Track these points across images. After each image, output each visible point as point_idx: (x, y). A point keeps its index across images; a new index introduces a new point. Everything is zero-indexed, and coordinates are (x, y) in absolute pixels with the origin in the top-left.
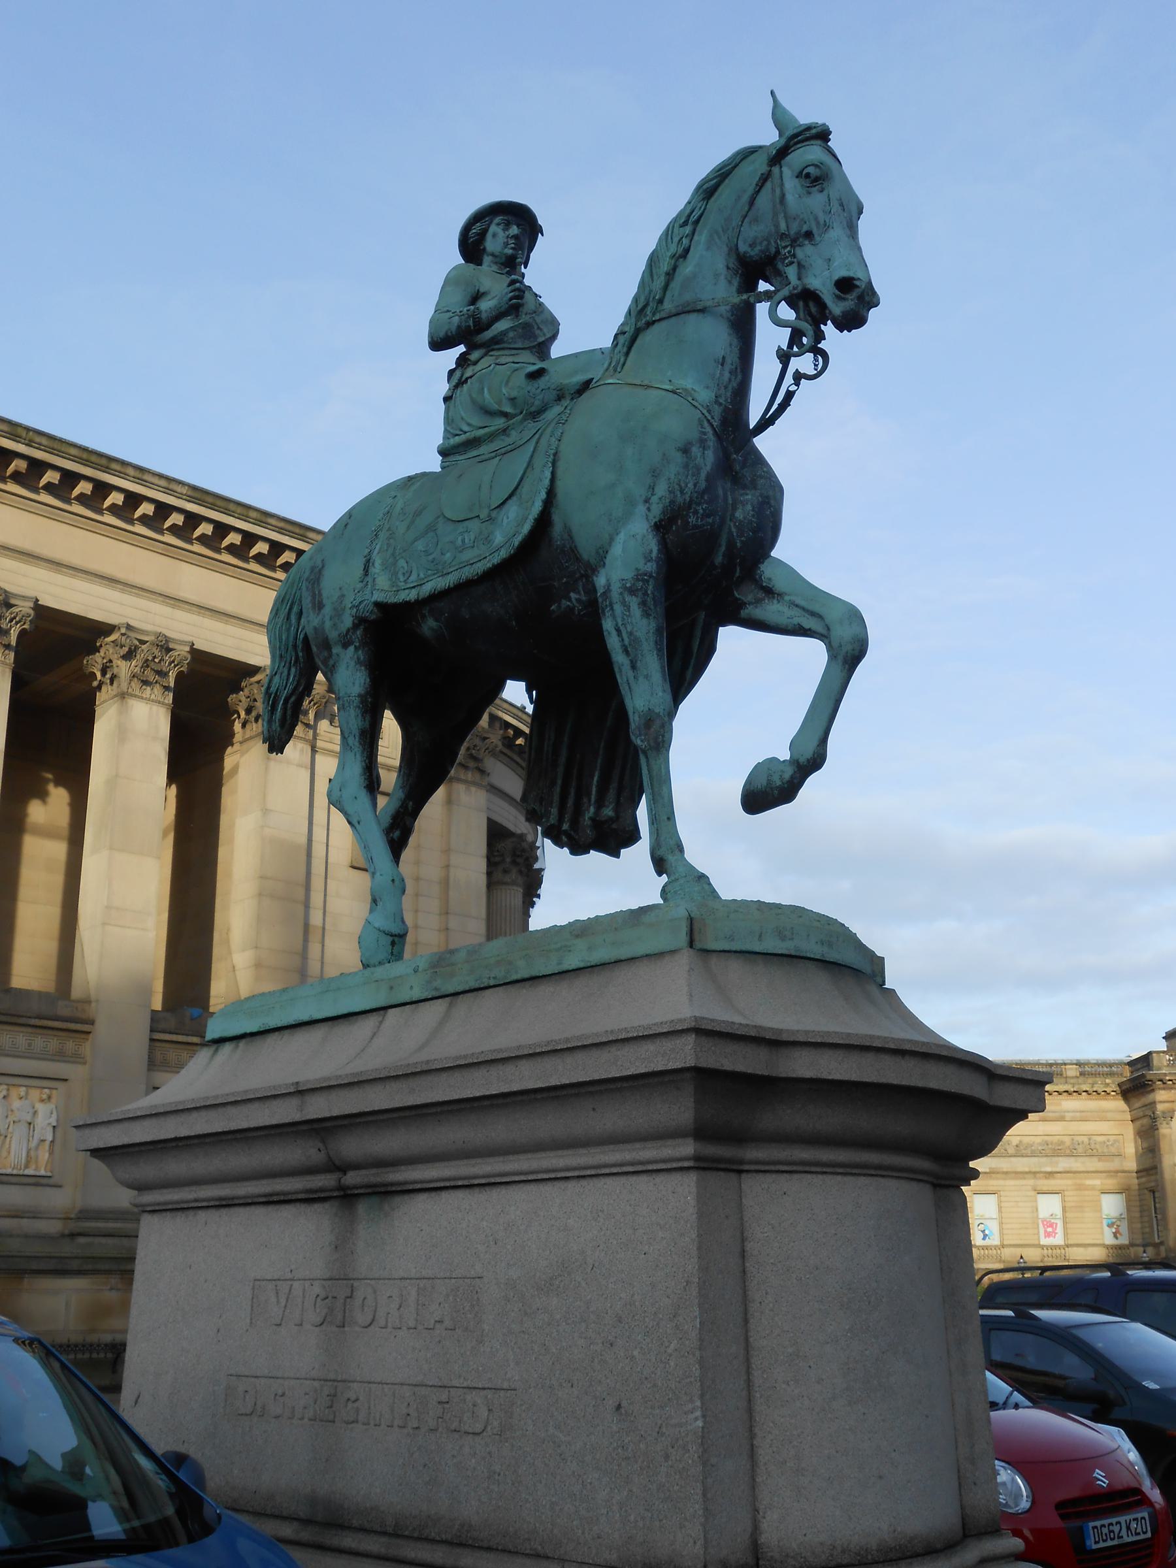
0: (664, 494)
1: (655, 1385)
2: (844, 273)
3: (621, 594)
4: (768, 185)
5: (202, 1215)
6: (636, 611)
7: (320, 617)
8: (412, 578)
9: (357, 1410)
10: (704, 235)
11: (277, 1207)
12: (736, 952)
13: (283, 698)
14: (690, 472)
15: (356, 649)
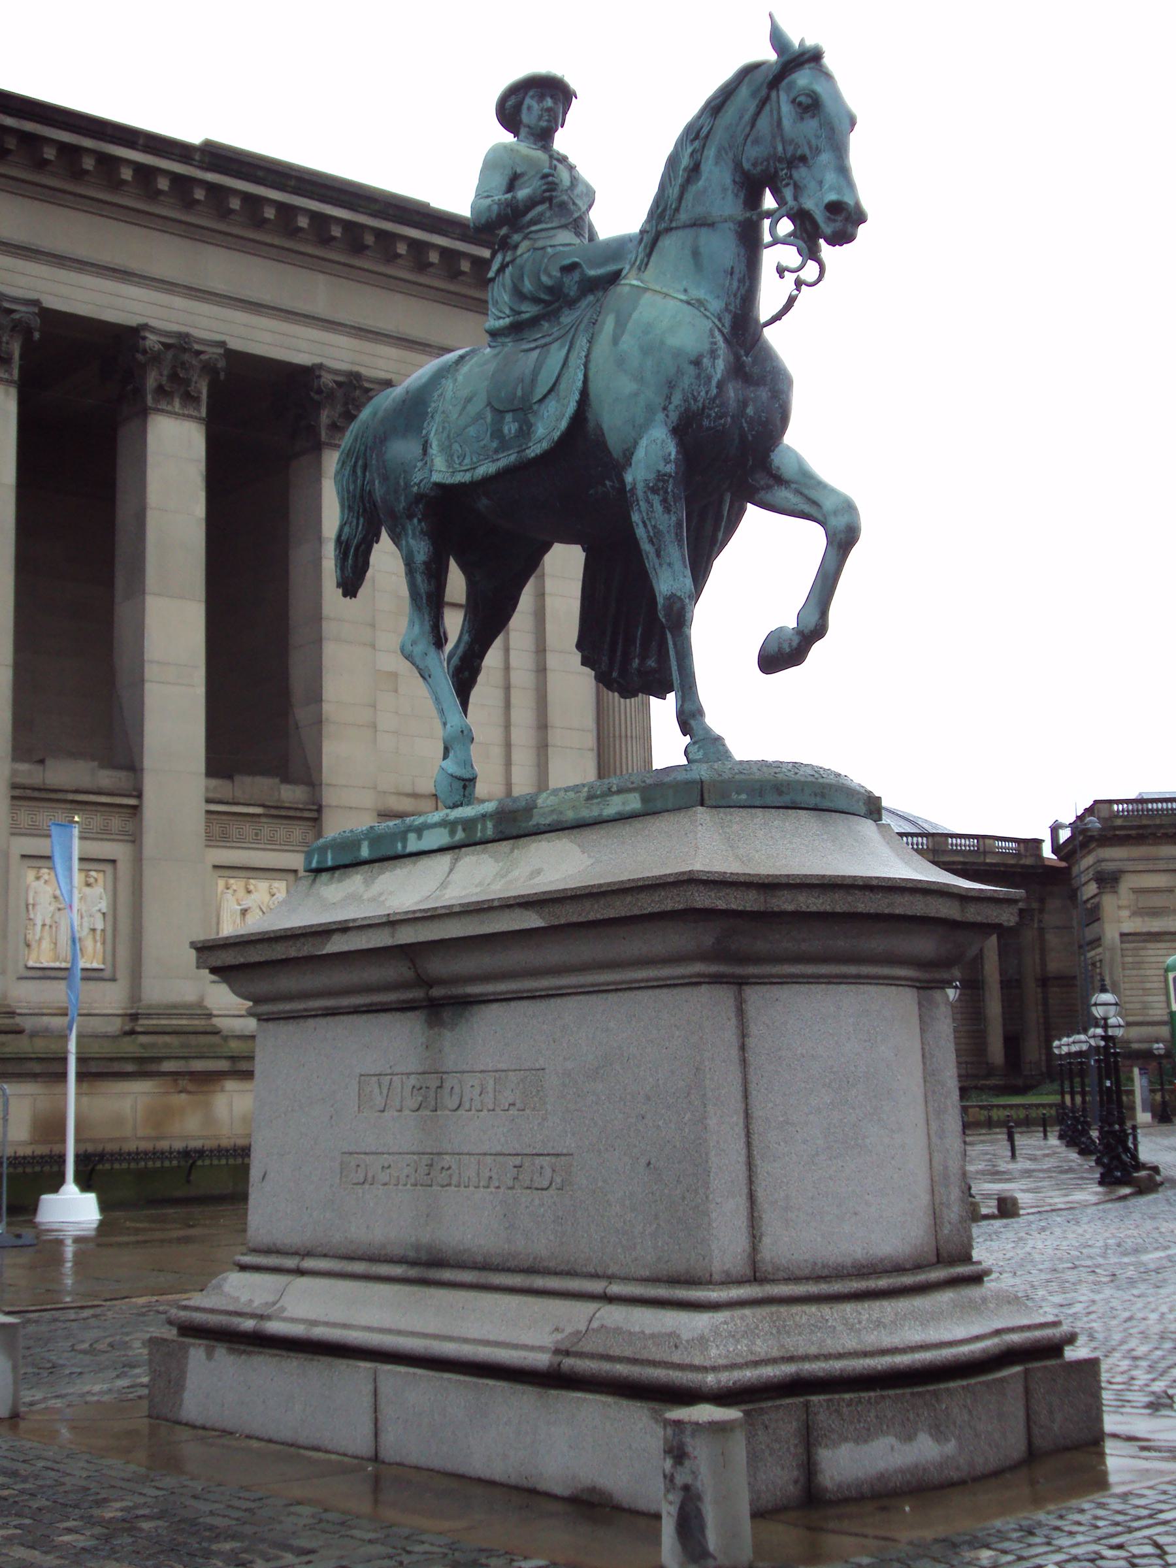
0: (679, 403)
1: (675, 1147)
2: (832, 197)
3: (645, 492)
4: (767, 108)
5: (311, 1022)
6: (658, 508)
9: (450, 1176)
10: (713, 150)
11: (376, 1015)
15: (420, 521)
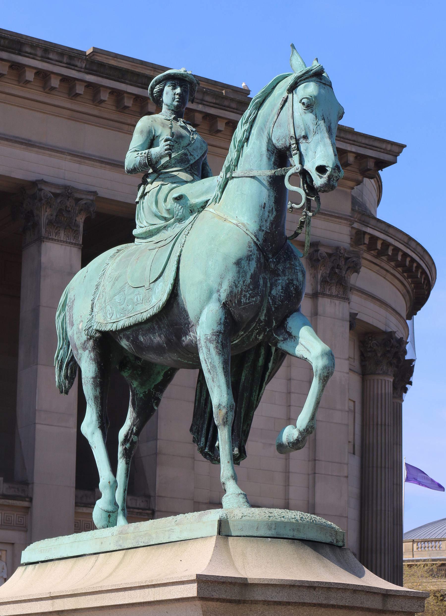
3: (205, 342)
7: (72, 330)
8: (112, 318)
12: (244, 536)
13: (65, 363)
14: (241, 275)
